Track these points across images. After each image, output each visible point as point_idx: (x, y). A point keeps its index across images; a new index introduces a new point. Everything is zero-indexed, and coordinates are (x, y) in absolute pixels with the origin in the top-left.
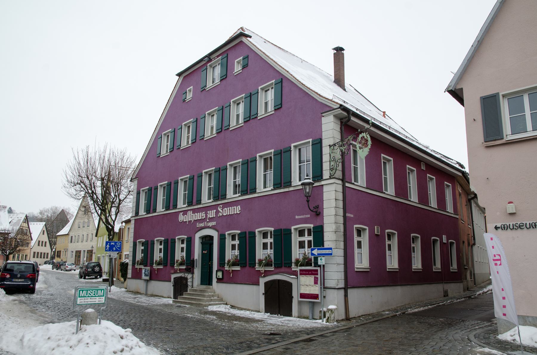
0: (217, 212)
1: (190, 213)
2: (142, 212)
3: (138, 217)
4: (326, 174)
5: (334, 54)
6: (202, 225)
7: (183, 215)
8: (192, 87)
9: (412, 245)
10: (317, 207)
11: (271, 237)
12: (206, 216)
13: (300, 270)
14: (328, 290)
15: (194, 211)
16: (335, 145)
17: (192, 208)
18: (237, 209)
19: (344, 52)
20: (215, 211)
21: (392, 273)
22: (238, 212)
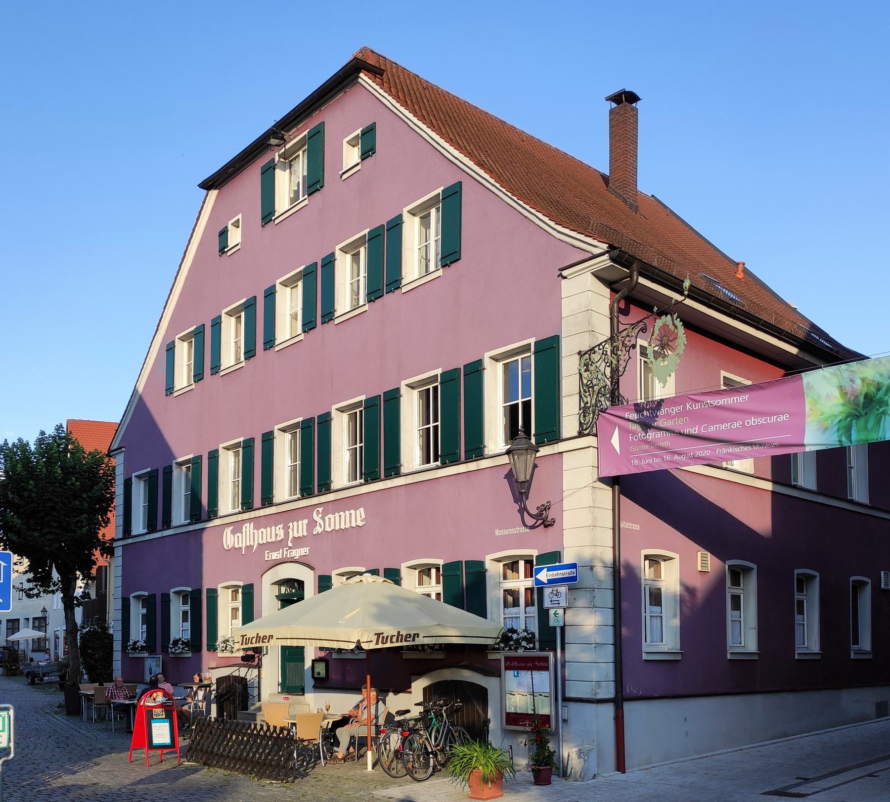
0: (312, 524)
1: (248, 528)
2: (139, 526)
3: (130, 541)
4: (569, 424)
5: (612, 112)
6: (276, 556)
7: (233, 532)
8: (240, 216)
9: (797, 597)
10: (546, 508)
11: (438, 582)
12: (287, 534)
13: (507, 659)
14: (572, 705)
15: (258, 523)
16: (592, 350)
17: (252, 514)
18: (356, 517)
19: (638, 105)
20: (305, 521)
21: (743, 664)
22: (360, 524)
